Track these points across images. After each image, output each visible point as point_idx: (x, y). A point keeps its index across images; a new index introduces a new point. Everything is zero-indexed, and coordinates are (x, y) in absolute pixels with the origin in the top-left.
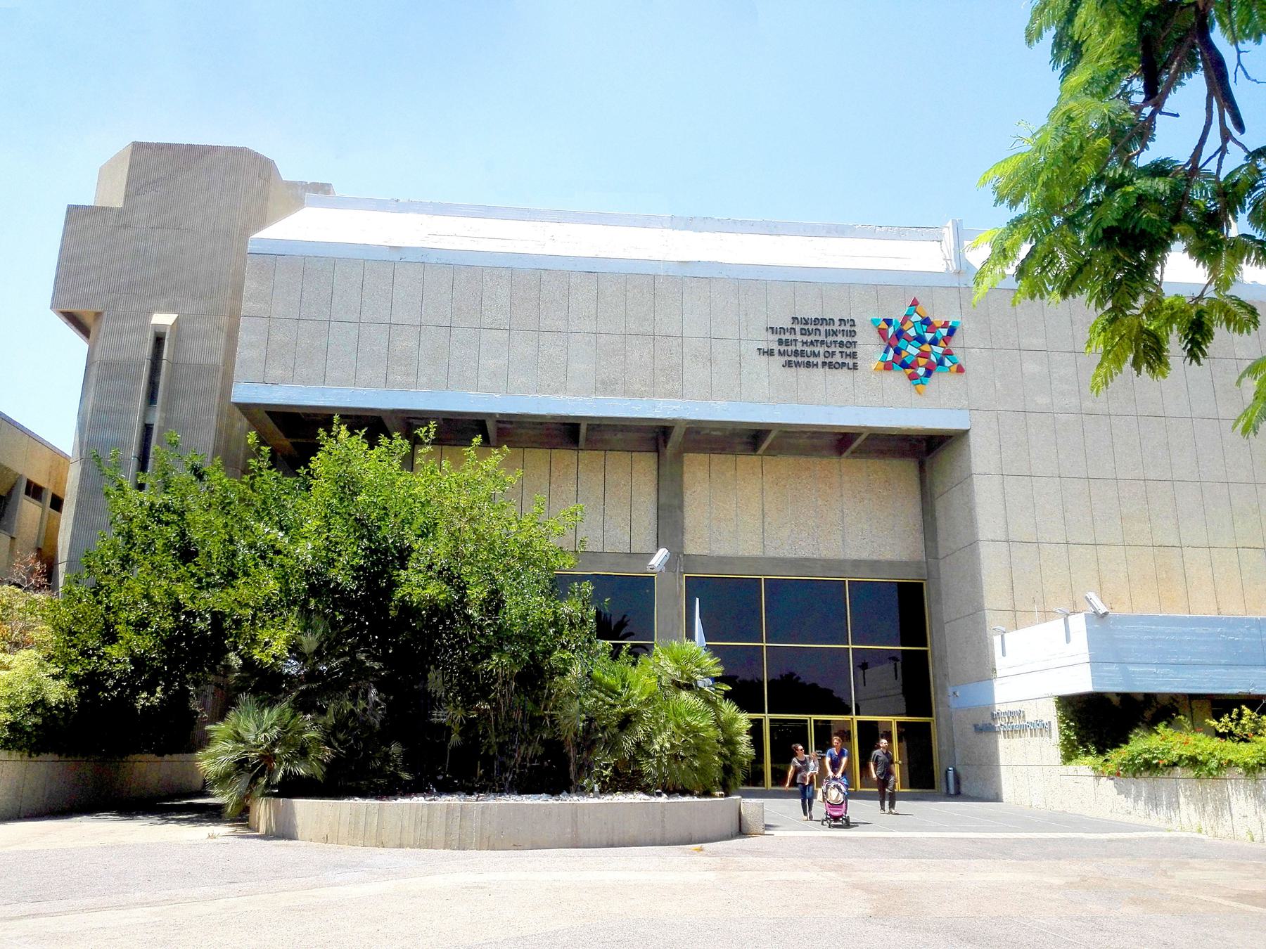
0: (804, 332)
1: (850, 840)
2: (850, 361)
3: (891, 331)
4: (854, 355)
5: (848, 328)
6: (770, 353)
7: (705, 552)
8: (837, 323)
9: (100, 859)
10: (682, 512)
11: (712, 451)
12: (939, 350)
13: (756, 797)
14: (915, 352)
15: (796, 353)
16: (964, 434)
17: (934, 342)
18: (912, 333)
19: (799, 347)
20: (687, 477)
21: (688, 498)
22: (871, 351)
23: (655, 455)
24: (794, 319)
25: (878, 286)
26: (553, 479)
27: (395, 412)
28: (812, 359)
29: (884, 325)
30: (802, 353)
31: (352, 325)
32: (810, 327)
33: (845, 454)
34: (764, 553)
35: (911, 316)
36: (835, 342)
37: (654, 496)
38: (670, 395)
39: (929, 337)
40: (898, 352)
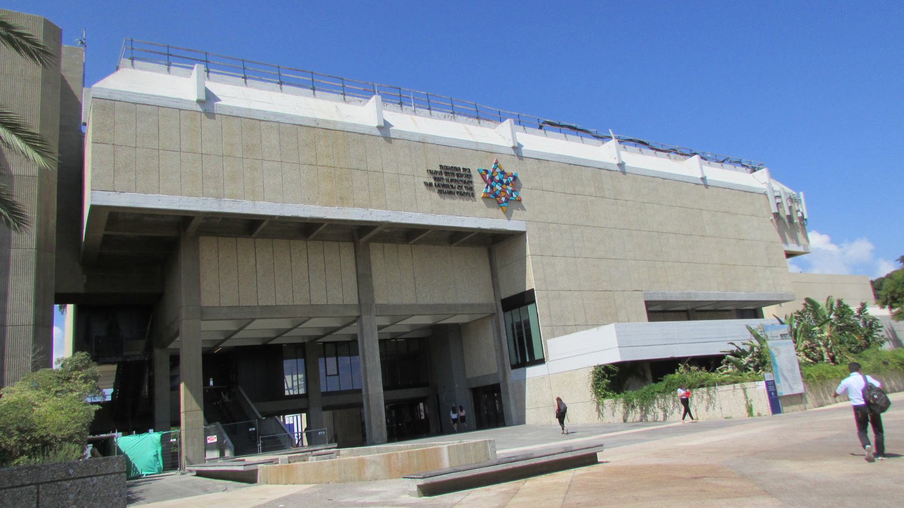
0: (446, 174)
1: (824, 411)
2: (470, 192)
3: (488, 176)
4: (471, 189)
5: (467, 173)
6: (430, 185)
7: (385, 302)
8: (462, 170)
9: (49, 492)
10: (371, 278)
11: (384, 241)
12: (510, 188)
13: (365, 429)
14: (500, 189)
15: (444, 186)
16: (522, 234)
17: (507, 184)
18: (497, 178)
19: (445, 183)
20: (372, 258)
21: (373, 268)
22: (480, 187)
23: (353, 243)
24: (441, 166)
25: (490, 152)
26: (293, 259)
27: (650, 155)
28: (452, 190)
29: (484, 172)
30: (447, 186)
31: (175, 153)
32: (450, 171)
33: (453, 245)
34: (417, 301)
35: (496, 169)
36: (462, 181)
37: (354, 269)
38: (379, 207)
39: (505, 181)
40: (492, 187)
